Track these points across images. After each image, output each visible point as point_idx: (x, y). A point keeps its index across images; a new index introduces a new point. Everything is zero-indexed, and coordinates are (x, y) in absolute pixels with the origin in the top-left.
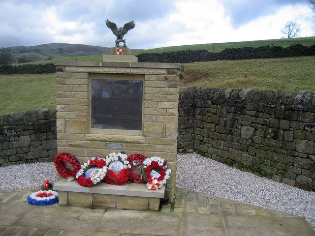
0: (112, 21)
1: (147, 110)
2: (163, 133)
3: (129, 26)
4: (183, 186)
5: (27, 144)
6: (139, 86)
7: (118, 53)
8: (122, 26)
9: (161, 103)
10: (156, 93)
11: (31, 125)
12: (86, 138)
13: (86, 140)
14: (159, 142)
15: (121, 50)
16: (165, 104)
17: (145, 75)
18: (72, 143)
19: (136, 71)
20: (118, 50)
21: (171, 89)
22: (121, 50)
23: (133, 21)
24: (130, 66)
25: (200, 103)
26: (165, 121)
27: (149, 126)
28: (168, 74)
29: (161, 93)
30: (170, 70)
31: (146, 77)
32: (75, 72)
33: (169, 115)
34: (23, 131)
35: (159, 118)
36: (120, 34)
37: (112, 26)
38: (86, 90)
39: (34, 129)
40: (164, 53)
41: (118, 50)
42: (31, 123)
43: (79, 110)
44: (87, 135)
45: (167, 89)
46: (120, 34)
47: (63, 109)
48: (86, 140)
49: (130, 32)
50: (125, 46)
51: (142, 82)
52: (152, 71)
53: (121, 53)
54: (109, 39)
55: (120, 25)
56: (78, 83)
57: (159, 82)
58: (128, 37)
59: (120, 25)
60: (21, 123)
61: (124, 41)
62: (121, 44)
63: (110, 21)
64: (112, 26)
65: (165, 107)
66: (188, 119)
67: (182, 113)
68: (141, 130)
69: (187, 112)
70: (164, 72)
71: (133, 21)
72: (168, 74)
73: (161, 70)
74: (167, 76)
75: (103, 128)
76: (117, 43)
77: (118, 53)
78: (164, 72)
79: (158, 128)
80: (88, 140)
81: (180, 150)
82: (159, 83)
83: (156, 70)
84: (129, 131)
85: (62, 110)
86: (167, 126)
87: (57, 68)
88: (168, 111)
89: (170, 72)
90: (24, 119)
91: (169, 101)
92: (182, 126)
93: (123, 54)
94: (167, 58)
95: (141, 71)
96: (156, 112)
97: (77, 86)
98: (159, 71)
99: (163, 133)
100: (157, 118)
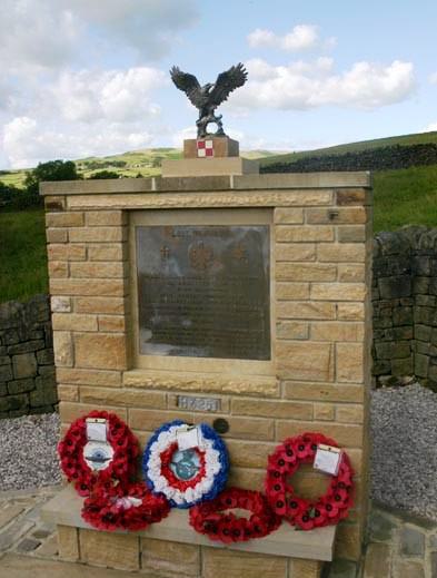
0: (185, 70)
1: (280, 306)
2: (330, 371)
3: (232, 79)
4: (395, 544)
5: (29, 371)
6: (259, 237)
7: (202, 153)
8: (213, 80)
9: (322, 286)
10: (307, 259)
11: (38, 329)
12: (125, 382)
13: (126, 386)
14: (318, 395)
15: (209, 144)
16: (334, 289)
17: (273, 208)
18: (96, 395)
19: (247, 200)
20: (202, 145)
21: (349, 246)
22: (209, 144)
23: (240, 66)
24: (232, 187)
25: (427, 265)
26: (334, 336)
27: (291, 349)
28: (339, 203)
29: (320, 257)
30: (343, 191)
31: (277, 217)
32: (92, 209)
33: (345, 319)
34: (20, 342)
35: (315, 326)
36: (209, 98)
37: (185, 82)
38: (120, 257)
39: (44, 338)
40: (348, 155)
41: (202, 145)
42: (36, 325)
43: (103, 310)
44: (131, 373)
45: (337, 244)
46: (209, 98)
47: (67, 306)
48: (126, 386)
49: (234, 94)
50: (221, 133)
51: (267, 230)
52: (292, 197)
53: (209, 152)
54: (178, 124)
55: (207, 78)
56: (100, 238)
57: (314, 227)
58: (233, 116)
59: (207, 78)
60: (15, 325)
61: (218, 120)
62: (212, 128)
63: (181, 70)
64: (185, 82)
65: (332, 298)
66: (400, 305)
67: (383, 289)
68: (269, 359)
69: (397, 287)
70: (326, 197)
71: (240, 66)
72: (339, 203)
73: (318, 192)
74: (335, 208)
75: (172, 353)
76: (202, 126)
77: (202, 153)
78: (326, 197)
79: (313, 356)
80: (131, 386)
81: (381, 378)
82: (313, 231)
83: (302, 193)
84: (237, 361)
85: (63, 309)
86: (339, 350)
87: (48, 200)
88: (340, 308)
89: (343, 197)
90: (21, 315)
91: (345, 278)
92: (387, 322)
93: (216, 156)
94: (355, 164)
95: (262, 199)
96: (306, 312)
97: (97, 246)
98: (310, 197)
99: (330, 371)
100: (309, 328)
